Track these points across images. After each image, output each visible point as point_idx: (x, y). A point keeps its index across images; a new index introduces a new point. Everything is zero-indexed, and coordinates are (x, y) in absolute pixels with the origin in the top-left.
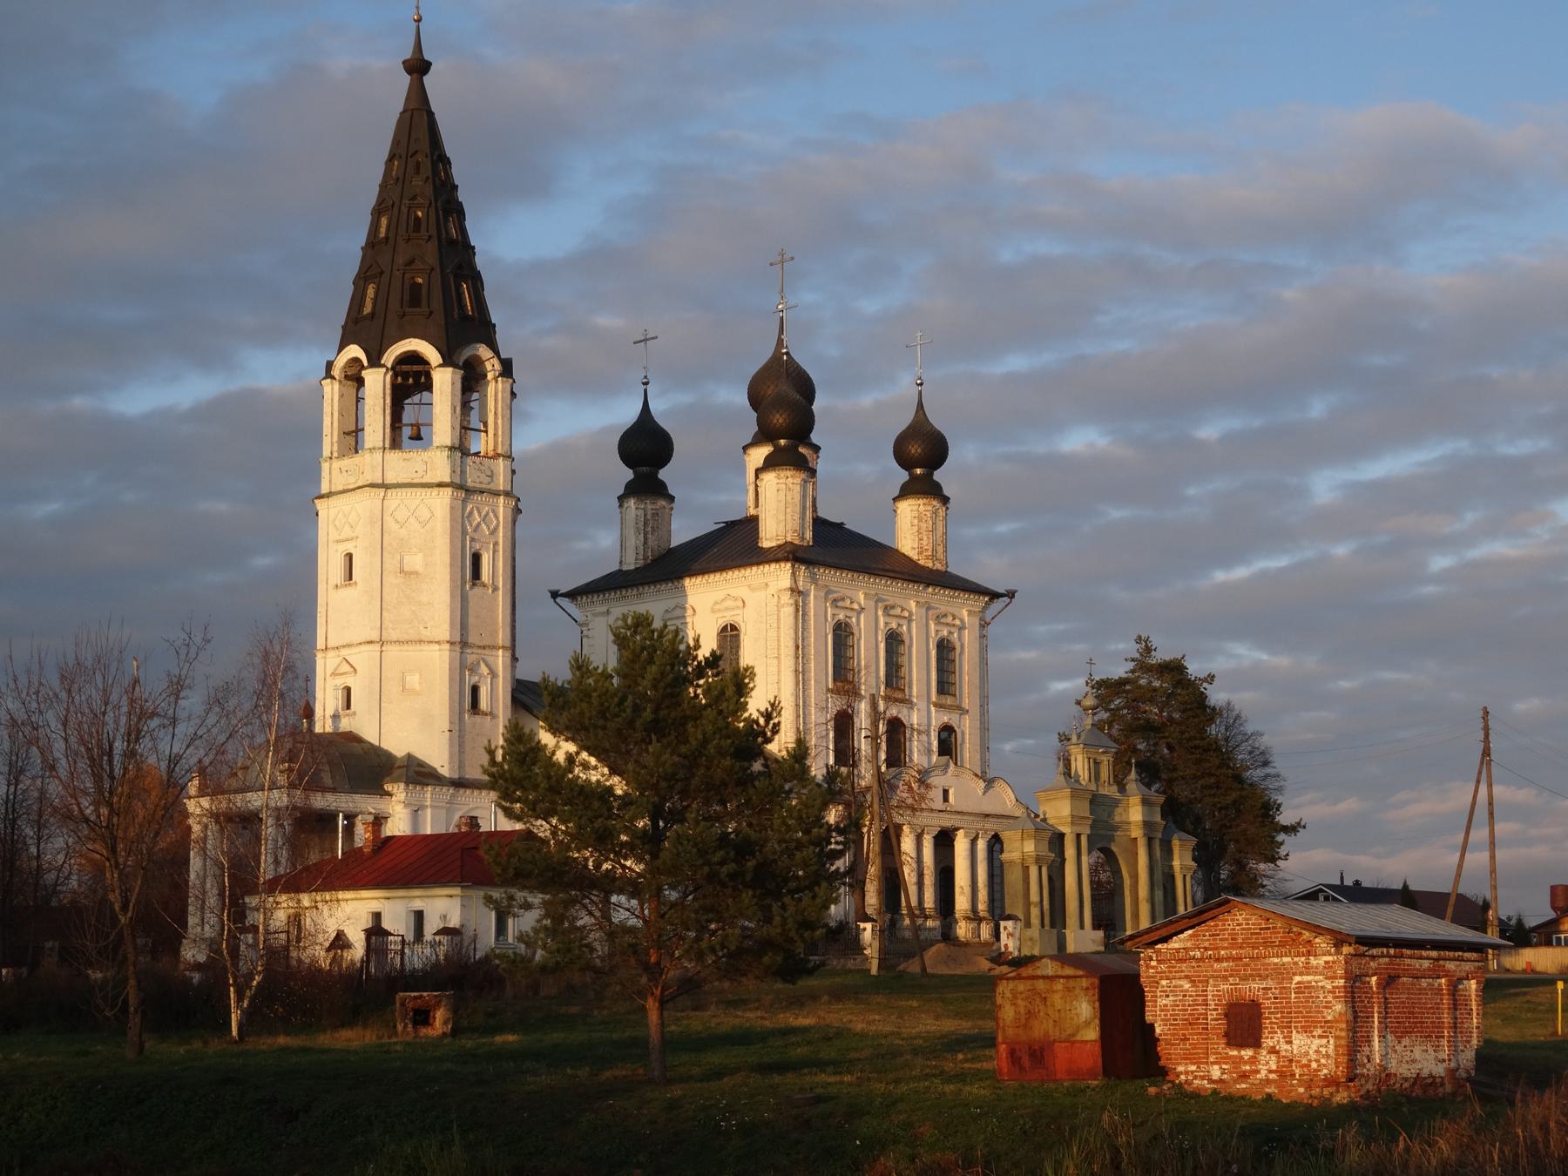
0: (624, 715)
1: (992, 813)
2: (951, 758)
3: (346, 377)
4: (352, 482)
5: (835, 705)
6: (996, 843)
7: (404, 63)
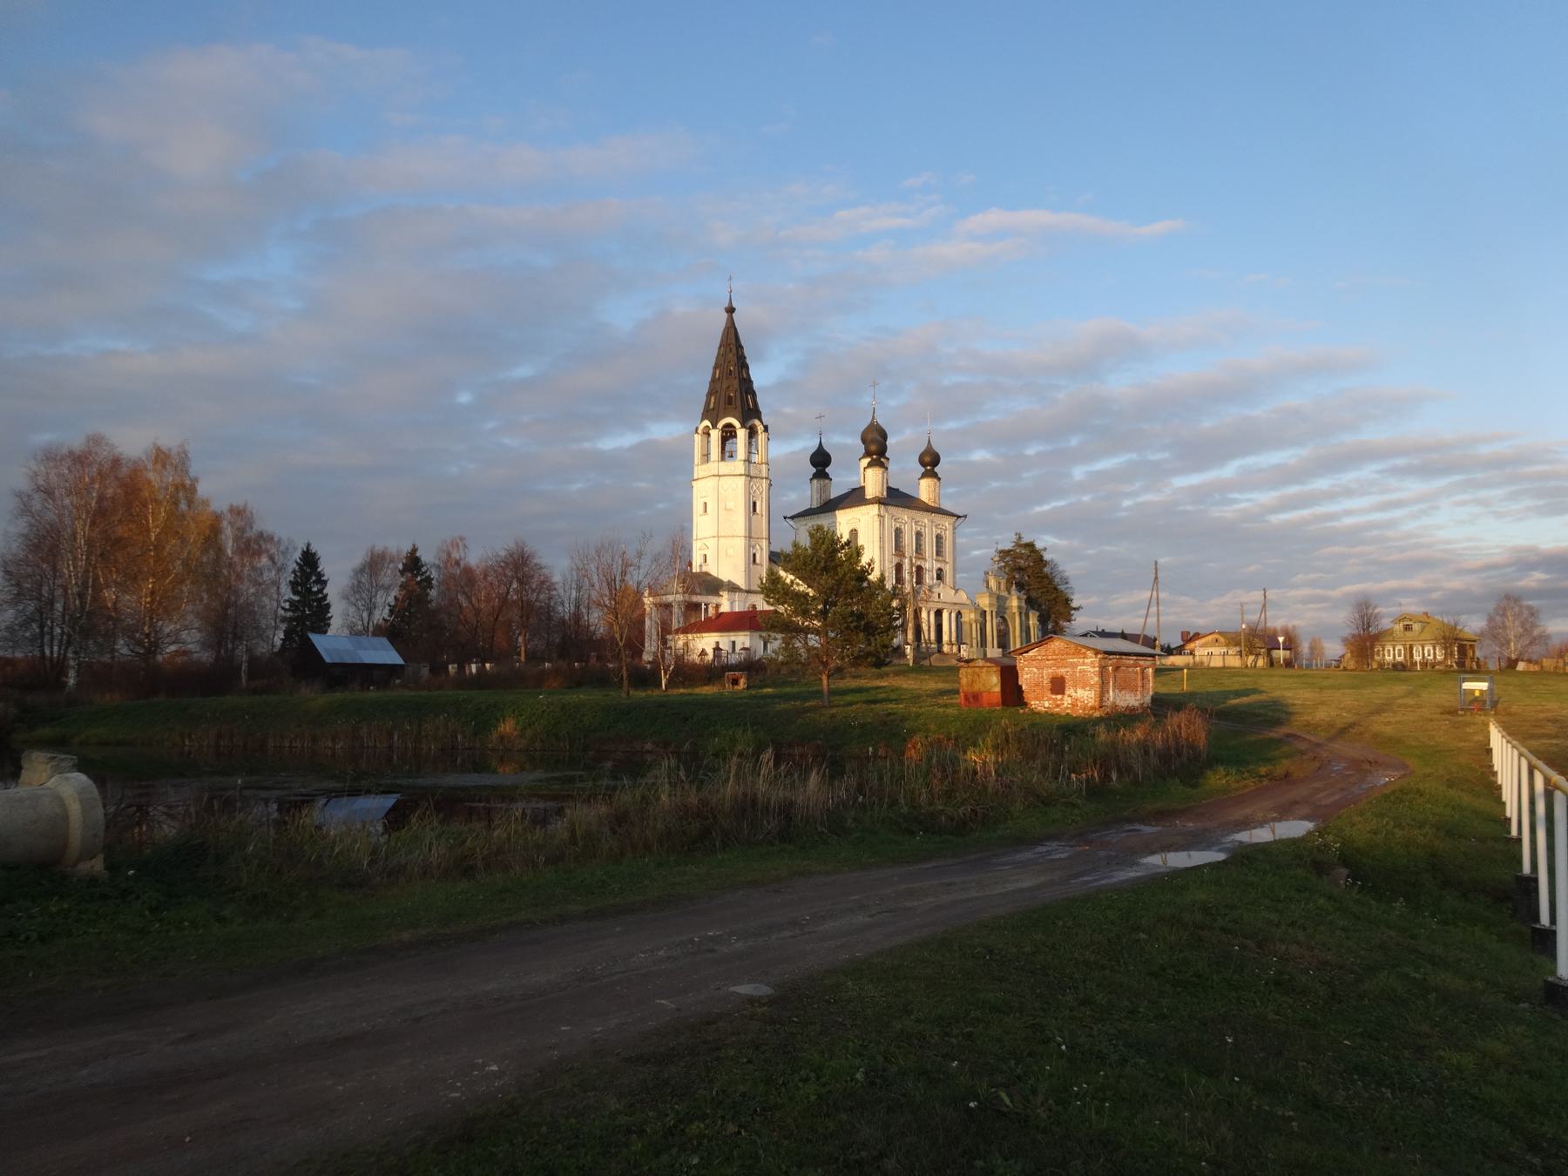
5: (896, 560)
6: (959, 614)
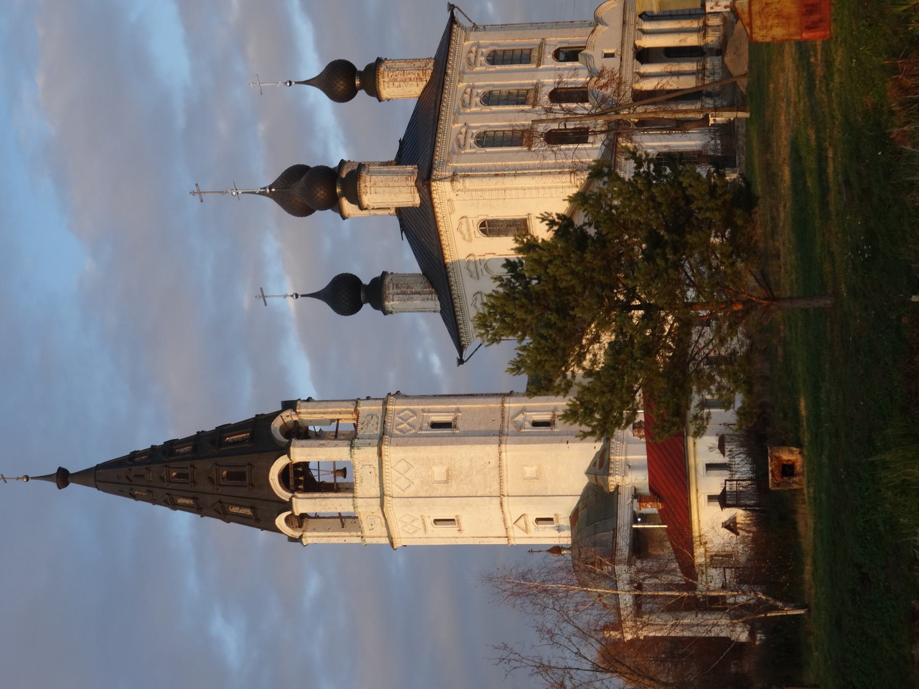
0: (554, 336)
1: (622, 18)
2: (581, 51)
3: (300, 526)
4: (380, 521)
5: (539, 145)
6: (646, 16)
7: (60, 488)
